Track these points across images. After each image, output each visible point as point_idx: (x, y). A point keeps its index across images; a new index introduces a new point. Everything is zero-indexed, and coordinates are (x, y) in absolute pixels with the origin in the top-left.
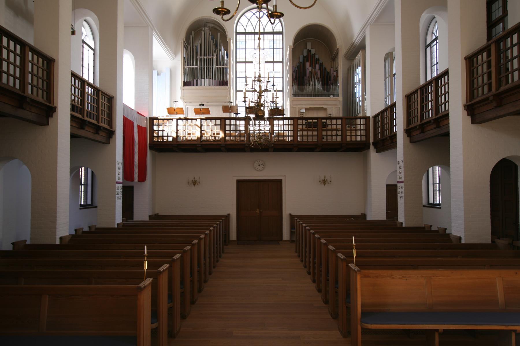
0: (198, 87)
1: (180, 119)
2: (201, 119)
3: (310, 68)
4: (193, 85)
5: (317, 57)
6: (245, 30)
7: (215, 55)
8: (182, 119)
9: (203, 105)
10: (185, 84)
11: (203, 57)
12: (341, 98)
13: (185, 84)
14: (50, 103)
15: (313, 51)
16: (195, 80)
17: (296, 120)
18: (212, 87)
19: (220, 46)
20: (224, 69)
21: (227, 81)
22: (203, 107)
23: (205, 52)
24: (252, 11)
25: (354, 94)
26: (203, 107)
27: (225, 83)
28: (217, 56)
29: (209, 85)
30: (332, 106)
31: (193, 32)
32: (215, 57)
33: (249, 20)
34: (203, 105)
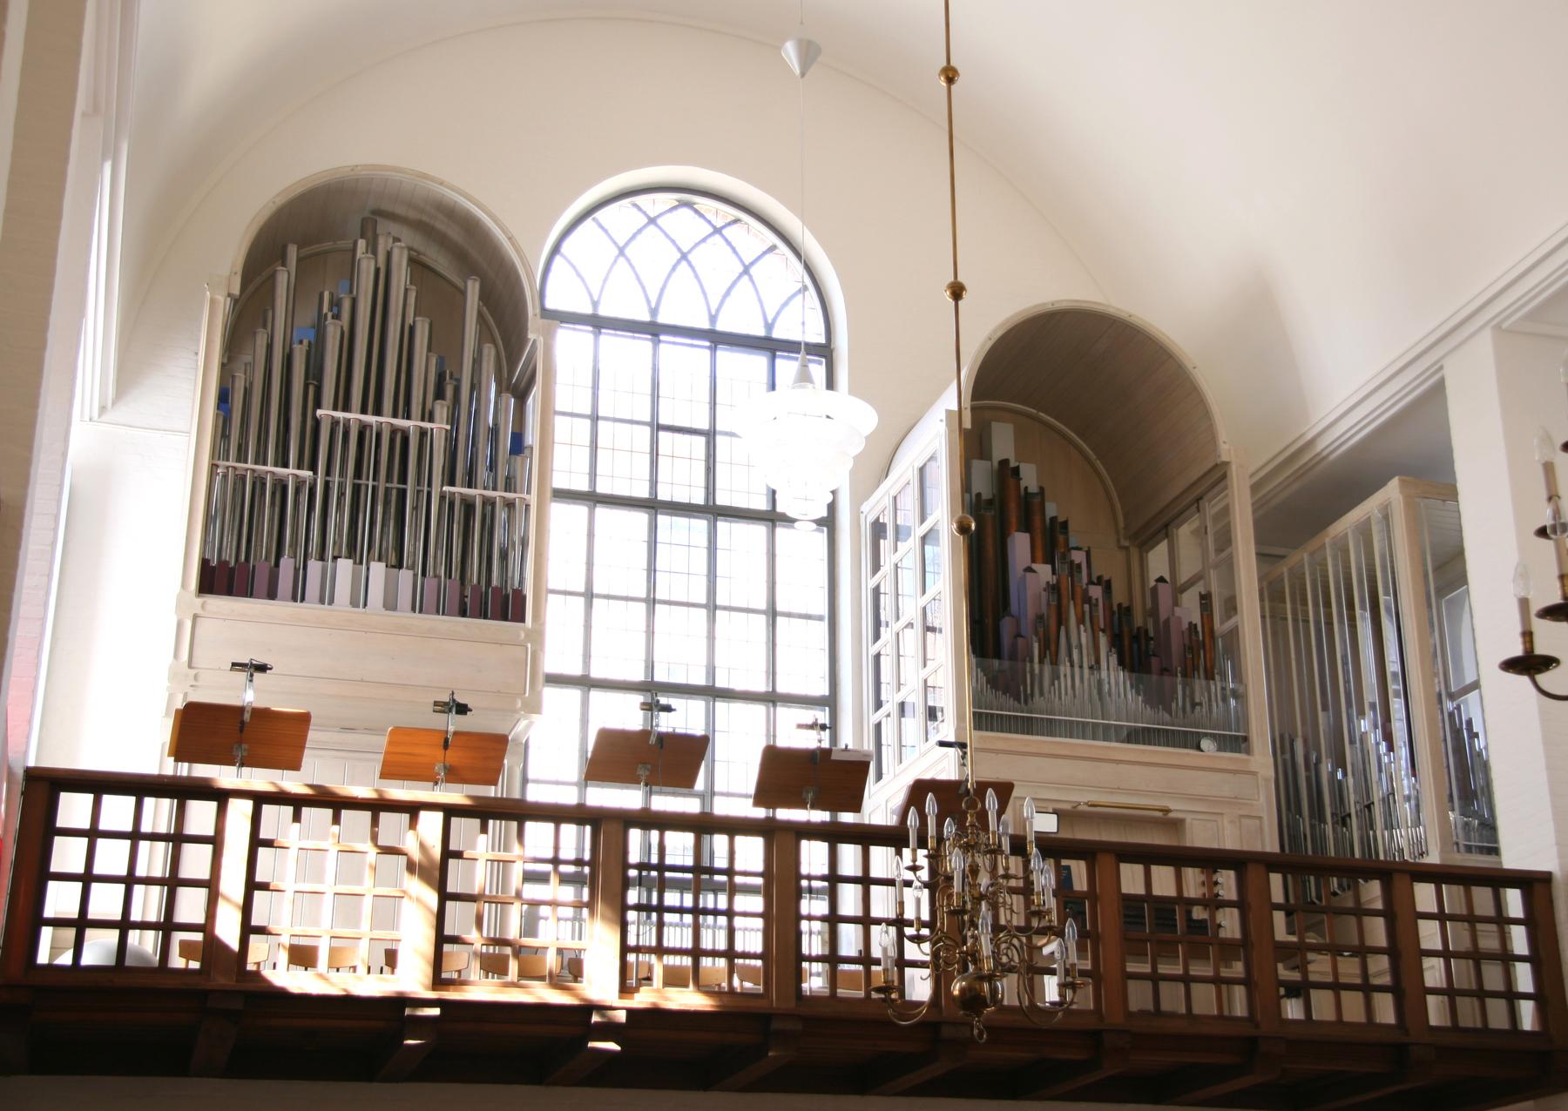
0: (309, 609)
1: (280, 798)
2: (450, 811)
3: (1044, 572)
4: (272, 594)
5: (1051, 510)
6: (595, 304)
7: (441, 410)
8: (297, 803)
9: (462, 709)
10: (217, 578)
11: (354, 416)
12: (1262, 760)
13: (217, 578)
14: (114, 404)
15: (1030, 478)
16: (287, 564)
17: (1105, 861)
18: (405, 617)
19: (477, 362)
20: (501, 515)
21: (520, 598)
22: (454, 723)
23: (375, 394)
24: (641, 200)
25: (823, 824)
26: (454, 723)
27: (507, 605)
28: (453, 420)
29: (390, 604)
30: (1224, 798)
31: (292, 252)
32: (439, 427)
33: (621, 252)
34: (462, 709)
